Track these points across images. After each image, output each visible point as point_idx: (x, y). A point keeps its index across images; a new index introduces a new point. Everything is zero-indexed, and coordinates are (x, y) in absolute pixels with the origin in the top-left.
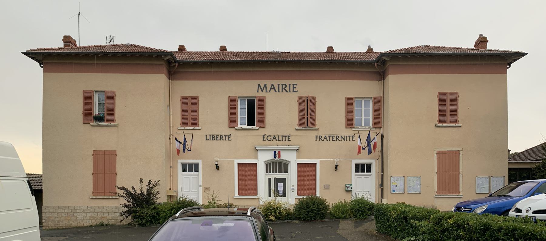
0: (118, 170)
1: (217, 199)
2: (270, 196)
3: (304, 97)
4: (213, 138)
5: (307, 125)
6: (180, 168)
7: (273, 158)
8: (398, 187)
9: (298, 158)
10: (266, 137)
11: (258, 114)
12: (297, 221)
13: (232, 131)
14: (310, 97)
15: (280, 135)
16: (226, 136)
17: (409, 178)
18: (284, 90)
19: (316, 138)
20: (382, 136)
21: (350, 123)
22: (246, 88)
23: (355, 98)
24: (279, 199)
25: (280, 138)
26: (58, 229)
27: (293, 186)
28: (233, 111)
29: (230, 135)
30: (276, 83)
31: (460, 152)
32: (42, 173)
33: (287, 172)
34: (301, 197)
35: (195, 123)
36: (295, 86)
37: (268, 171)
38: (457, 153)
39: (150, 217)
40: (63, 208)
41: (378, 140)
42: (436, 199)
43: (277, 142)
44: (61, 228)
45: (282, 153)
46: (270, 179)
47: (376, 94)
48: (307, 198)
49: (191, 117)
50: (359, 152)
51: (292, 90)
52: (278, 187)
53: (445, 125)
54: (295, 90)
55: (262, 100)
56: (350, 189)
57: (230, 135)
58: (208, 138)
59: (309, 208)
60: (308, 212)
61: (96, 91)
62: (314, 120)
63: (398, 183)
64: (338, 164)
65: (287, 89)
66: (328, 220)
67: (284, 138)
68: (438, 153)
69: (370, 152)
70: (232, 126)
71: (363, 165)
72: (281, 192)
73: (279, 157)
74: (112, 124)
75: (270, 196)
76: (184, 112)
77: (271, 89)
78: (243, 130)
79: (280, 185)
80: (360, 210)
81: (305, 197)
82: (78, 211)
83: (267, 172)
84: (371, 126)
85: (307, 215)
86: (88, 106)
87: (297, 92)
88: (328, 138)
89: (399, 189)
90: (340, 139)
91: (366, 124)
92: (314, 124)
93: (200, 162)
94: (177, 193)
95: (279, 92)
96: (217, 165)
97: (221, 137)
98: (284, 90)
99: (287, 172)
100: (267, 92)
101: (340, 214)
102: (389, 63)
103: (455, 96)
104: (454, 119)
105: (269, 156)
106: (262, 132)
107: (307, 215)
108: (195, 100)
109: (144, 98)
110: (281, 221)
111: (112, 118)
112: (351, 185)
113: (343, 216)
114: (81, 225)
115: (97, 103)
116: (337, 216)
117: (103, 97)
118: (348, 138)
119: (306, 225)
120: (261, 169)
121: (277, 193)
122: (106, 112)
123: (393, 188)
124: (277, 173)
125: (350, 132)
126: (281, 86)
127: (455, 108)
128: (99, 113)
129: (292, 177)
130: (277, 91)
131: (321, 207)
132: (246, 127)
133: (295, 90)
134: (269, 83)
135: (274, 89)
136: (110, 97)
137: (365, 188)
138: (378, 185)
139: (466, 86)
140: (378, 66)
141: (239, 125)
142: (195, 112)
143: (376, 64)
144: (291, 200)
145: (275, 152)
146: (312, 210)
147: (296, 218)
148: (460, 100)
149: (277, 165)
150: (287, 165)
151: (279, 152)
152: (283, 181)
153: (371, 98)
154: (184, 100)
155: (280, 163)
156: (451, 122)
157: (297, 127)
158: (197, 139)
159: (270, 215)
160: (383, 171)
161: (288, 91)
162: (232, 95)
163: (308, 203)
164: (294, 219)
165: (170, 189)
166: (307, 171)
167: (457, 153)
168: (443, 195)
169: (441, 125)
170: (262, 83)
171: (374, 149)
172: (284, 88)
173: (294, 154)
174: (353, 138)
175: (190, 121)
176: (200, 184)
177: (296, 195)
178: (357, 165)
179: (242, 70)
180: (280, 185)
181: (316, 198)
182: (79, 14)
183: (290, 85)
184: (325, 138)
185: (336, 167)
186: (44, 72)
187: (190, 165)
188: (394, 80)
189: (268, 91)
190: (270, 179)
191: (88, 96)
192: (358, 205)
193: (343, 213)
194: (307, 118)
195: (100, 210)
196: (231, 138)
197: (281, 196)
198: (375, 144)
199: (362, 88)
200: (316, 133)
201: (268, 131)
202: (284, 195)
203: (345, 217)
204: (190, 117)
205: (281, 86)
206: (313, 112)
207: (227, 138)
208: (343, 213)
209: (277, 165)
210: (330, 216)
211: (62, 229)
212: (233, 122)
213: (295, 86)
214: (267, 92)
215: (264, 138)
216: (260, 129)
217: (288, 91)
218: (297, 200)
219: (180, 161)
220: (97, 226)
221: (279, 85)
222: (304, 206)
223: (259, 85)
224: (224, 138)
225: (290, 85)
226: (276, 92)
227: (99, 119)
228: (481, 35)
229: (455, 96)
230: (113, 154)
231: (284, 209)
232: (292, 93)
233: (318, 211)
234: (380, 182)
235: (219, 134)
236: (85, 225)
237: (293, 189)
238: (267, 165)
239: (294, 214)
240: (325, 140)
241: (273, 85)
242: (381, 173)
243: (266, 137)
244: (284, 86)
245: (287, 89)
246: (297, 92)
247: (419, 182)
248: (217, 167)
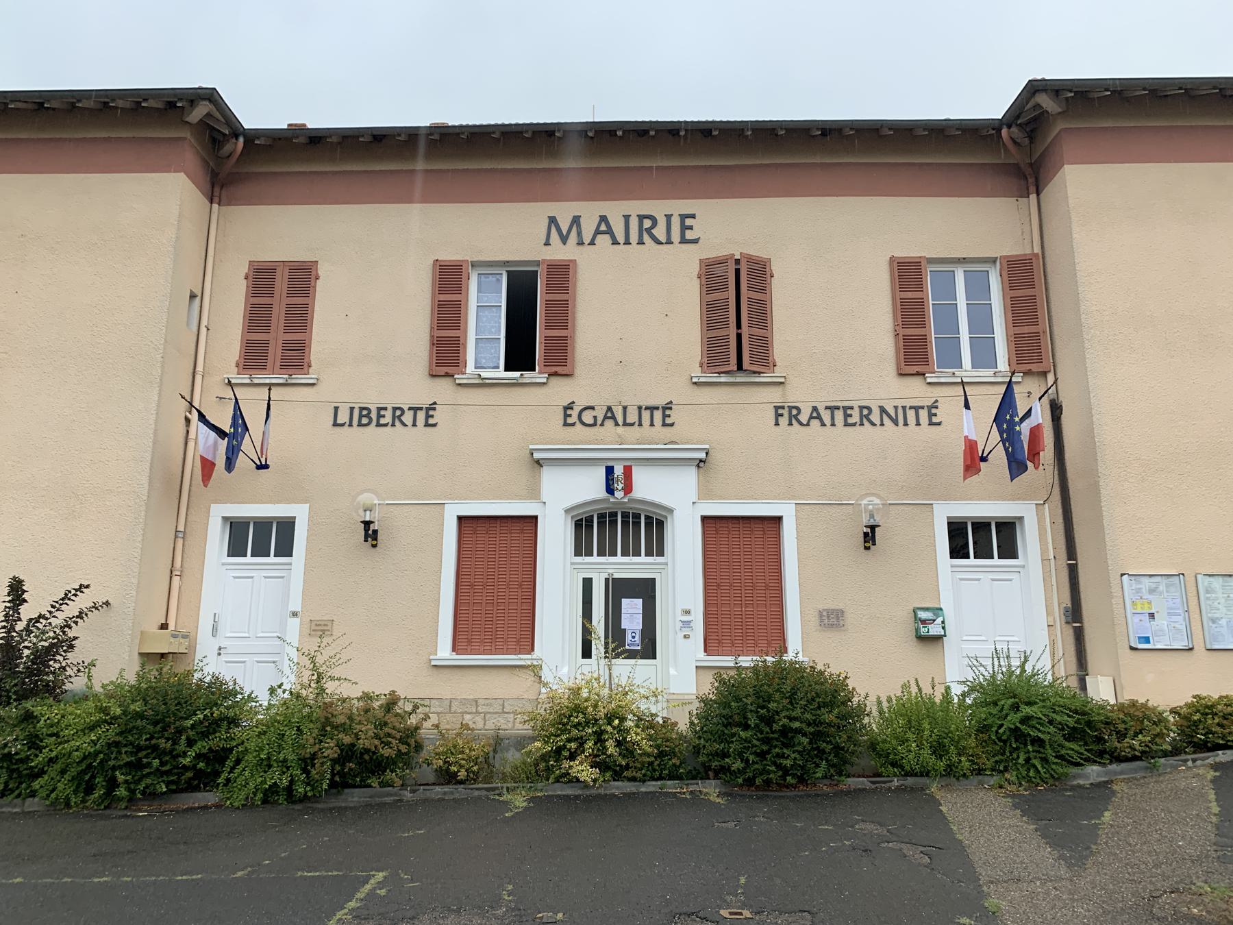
1: (336, 672)
2: (587, 653)
3: (722, 261)
6: (216, 538)
7: (601, 493)
8: (1161, 621)
9: (705, 493)
11: (548, 326)
12: (711, 790)
13: (441, 391)
14: (751, 260)
15: (633, 401)
16: (415, 410)
18: (646, 237)
19: (778, 416)
21: (913, 355)
22: (503, 230)
23: (931, 261)
25: (632, 417)
27: (687, 612)
29: (432, 407)
30: (615, 211)
33: (661, 553)
34: (727, 661)
35: (296, 358)
36: (688, 222)
41: (1040, 415)
43: (621, 430)
45: (638, 474)
46: (587, 583)
48: (755, 669)
51: (676, 236)
54: (689, 235)
55: (562, 274)
56: (935, 630)
57: (432, 407)
58: (343, 417)
59: (769, 721)
60: (766, 741)
64: (878, 519)
65: (660, 232)
66: (864, 782)
67: (646, 415)
69: (1017, 466)
70: (443, 370)
71: (981, 527)
72: (634, 639)
73: (628, 489)
75: (587, 653)
76: (257, 318)
77: (598, 232)
78: (484, 384)
79: (632, 609)
81: (746, 661)
83: (578, 553)
84: (1003, 365)
85: (762, 755)
90: (875, 417)
91: (984, 356)
92: (764, 359)
93: (300, 513)
94: (192, 647)
95: (627, 243)
96: (367, 524)
99: (661, 553)
100: (581, 243)
105: (586, 487)
106: (561, 391)
107: (762, 755)
108: (303, 277)
110: (629, 787)
113: (941, 764)
116: (910, 760)
118: (911, 414)
119: (762, 818)
120: (555, 539)
121: (617, 644)
123: (1137, 626)
124: (619, 558)
125: (914, 391)
126: (634, 223)
129: (681, 573)
130: (621, 239)
131: (830, 717)
132: (501, 373)
133: (689, 235)
134: (590, 212)
135: (610, 232)
137: (997, 625)
138: (1058, 617)
141: (470, 368)
143: (1004, 131)
144: (676, 680)
145: (610, 471)
146: (785, 731)
147: (701, 773)
149: (621, 524)
150: (661, 524)
151: (628, 471)
152: (645, 590)
153: (993, 261)
154: (262, 277)
155: (632, 519)
157: (697, 373)
158: (291, 423)
159: (572, 757)
160: (1071, 552)
161: (663, 238)
162: (449, 255)
163: (763, 698)
164: (694, 776)
165: (164, 626)
166: (743, 550)
170: (564, 212)
173: (689, 478)
175: (275, 352)
177: (701, 654)
178: (956, 530)
179: (487, 165)
180: (632, 609)
181: (796, 670)
184: (815, 414)
187: (263, 525)
189: (587, 240)
190: (587, 583)
192: (1016, 708)
194: (739, 336)
196: (438, 416)
197: (632, 655)
200: (774, 396)
201: (580, 389)
202: (649, 650)
204: (277, 337)
205: (634, 223)
206: (762, 315)
207: (421, 416)
208: (939, 750)
209: (621, 524)
212: (446, 355)
213: (688, 222)
214: (581, 243)
215: (787, 414)
216: (554, 380)
217: (663, 238)
218: (709, 678)
219: (220, 511)
221: (627, 218)
222: (743, 711)
223: (553, 220)
224: (408, 418)
226: (615, 242)
231: (647, 723)
232: (677, 247)
233: (816, 736)
234: (1067, 602)
237: (686, 624)
238: (578, 524)
240: (815, 423)
241: (603, 219)
242: (1063, 561)
243: (574, 413)
245: (660, 232)
246: (696, 241)
248: (371, 534)
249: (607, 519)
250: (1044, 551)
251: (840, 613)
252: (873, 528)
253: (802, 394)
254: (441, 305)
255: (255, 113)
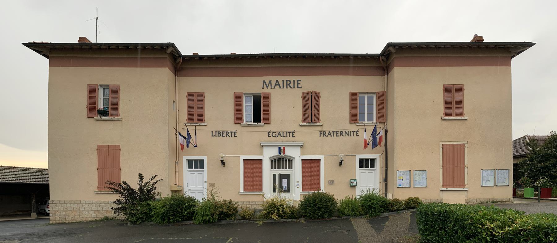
0: (122, 166)
1: (217, 195)
3: (308, 93)
4: (219, 134)
5: (312, 121)
6: (185, 165)
7: (278, 154)
9: (302, 154)
10: (271, 134)
12: (303, 220)
13: (237, 128)
15: (285, 131)
16: (231, 132)
17: (415, 172)
18: (288, 86)
19: (321, 134)
20: (386, 132)
21: (354, 118)
24: (283, 195)
25: (285, 135)
26: (64, 223)
28: (238, 108)
29: (235, 132)
30: (280, 79)
31: (466, 145)
32: (46, 167)
33: (292, 168)
34: (306, 193)
35: (201, 119)
36: (299, 82)
37: (273, 167)
38: (462, 146)
39: (142, 214)
40: (69, 202)
41: (382, 133)
42: (441, 192)
44: (67, 222)
45: (286, 149)
46: (274, 175)
47: (380, 90)
48: (313, 194)
49: (197, 113)
50: (365, 147)
51: (296, 86)
52: (283, 184)
53: (451, 118)
54: (299, 86)
55: (267, 96)
56: (354, 184)
57: (235, 132)
58: (214, 134)
59: (315, 205)
60: (315, 210)
61: (101, 86)
62: (318, 115)
63: (404, 177)
64: (343, 159)
66: (336, 218)
67: (288, 134)
68: (444, 147)
71: (367, 160)
72: (285, 188)
73: (284, 153)
74: (116, 118)
75: (274, 191)
76: (190, 108)
77: (276, 85)
79: (285, 181)
80: (375, 209)
81: (311, 192)
82: (84, 206)
85: (314, 213)
86: (92, 100)
87: (301, 87)
88: (332, 134)
89: (406, 183)
90: (344, 134)
91: (370, 118)
92: (318, 120)
93: (205, 158)
94: (183, 189)
95: (283, 88)
96: (222, 161)
97: (227, 133)
98: (288, 86)
99: (292, 168)
101: (350, 212)
102: (394, 56)
103: (460, 89)
104: (460, 111)
105: (274, 152)
106: (267, 128)
107: (314, 213)
108: (201, 97)
109: (148, 93)
110: (285, 220)
111: (116, 112)
112: (355, 180)
113: (353, 213)
114: (87, 219)
115: (103, 98)
117: (107, 91)
118: (352, 133)
120: (267, 165)
121: (281, 189)
122: (110, 107)
123: (399, 182)
124: (282, 170)
125: (353, 127)
126: (285, 82)
127: (460, 101)
128: (103, 107)
130: (282, 87)
131: (329, 204)
133: (299, 86)
134: (274, 79)
135: (279, 85)
136: (114, 91)
137: (368, 183)
139: (473, 79)
140: (398, 54)
141: (245, 122)
142: (201, 108)
143: (380, 58)
144: (295, 196)
145: (280, 148)
146: (319, 207)
147: (301, 217)
148: (465, 93)
150: (292, 161)
151: (284, 148)
152: (288, 177)
153: (375, 93)
155: (285, 160)
156: (456, 115)
157: (301, 123)
159: (272, 214)
160: (386, 166)
161: (292, 86)
163: (314, 200)
164: (299, 218)
165: (176, 184)
166: (311, 167)
167: (462, 146)
168: (449, 189)
169: (447, 118)
170: (267, 79)
171: (380, 143)
172: (289, 84)
173: (298, 150)
174: (357, 133)
175: (196, 117)
176: (206, 180)
177: (301, 191)
178: (361, 161)
180: (285, 181)
181: (323, 194)
182: (97, 19)
183: (294, 81)
184: (329, 133)
185: (341, 163)
186: (50, 65)
187: (196, 161)
188: (399, 72)
190: (274, 175)
191: (92, 90)
192: (370, 201)
193: (353, 210)
195: (105, 205)
196: (237, 134)
197: (285, 191)
198: (381, 137)
199: (367, 83)
200: (320, 129)
201: (273, 127)
202: (289, 190)
203: (355, 215)
204: (196, 113)
205: (285, 82)
206: (318, 107)
207: (233, 134)
208: (353, 210)
210: (337, 213)
211: (69, 223)
212: (238, 118)
213: (299, 82)
215: (323, 133)
216: (266, 125)
217: (292, 86)
219: (185, 158)
220: (102, 220)
221: (283, 81)
222: (310, 203)
223: (264, 82)
224: (230, 134)
225: (294, 81)
227: (104, 113)
228: (476, 36)
229: (460, 89)
230: (117, 149)
232: (296, 89)
233: (326, 208)
235: (225, 130)
236: (91, 219)
237: (298, 184)
238: (272, 161)
239: (299, 212)
240: (329, 136)
241: (277, 81)
242: (385, 168)
243: (271, 134)
244: (289, 82)
245: (292, 85)
246: (301, 87)
247: (425, 176)
248: (223, 163)
249: (279, 160)
250: (380, 165)
251: (333, 181)
252: (342, 161)
253: (326, 129)
254: (236, 105)
255: (185, 50)
